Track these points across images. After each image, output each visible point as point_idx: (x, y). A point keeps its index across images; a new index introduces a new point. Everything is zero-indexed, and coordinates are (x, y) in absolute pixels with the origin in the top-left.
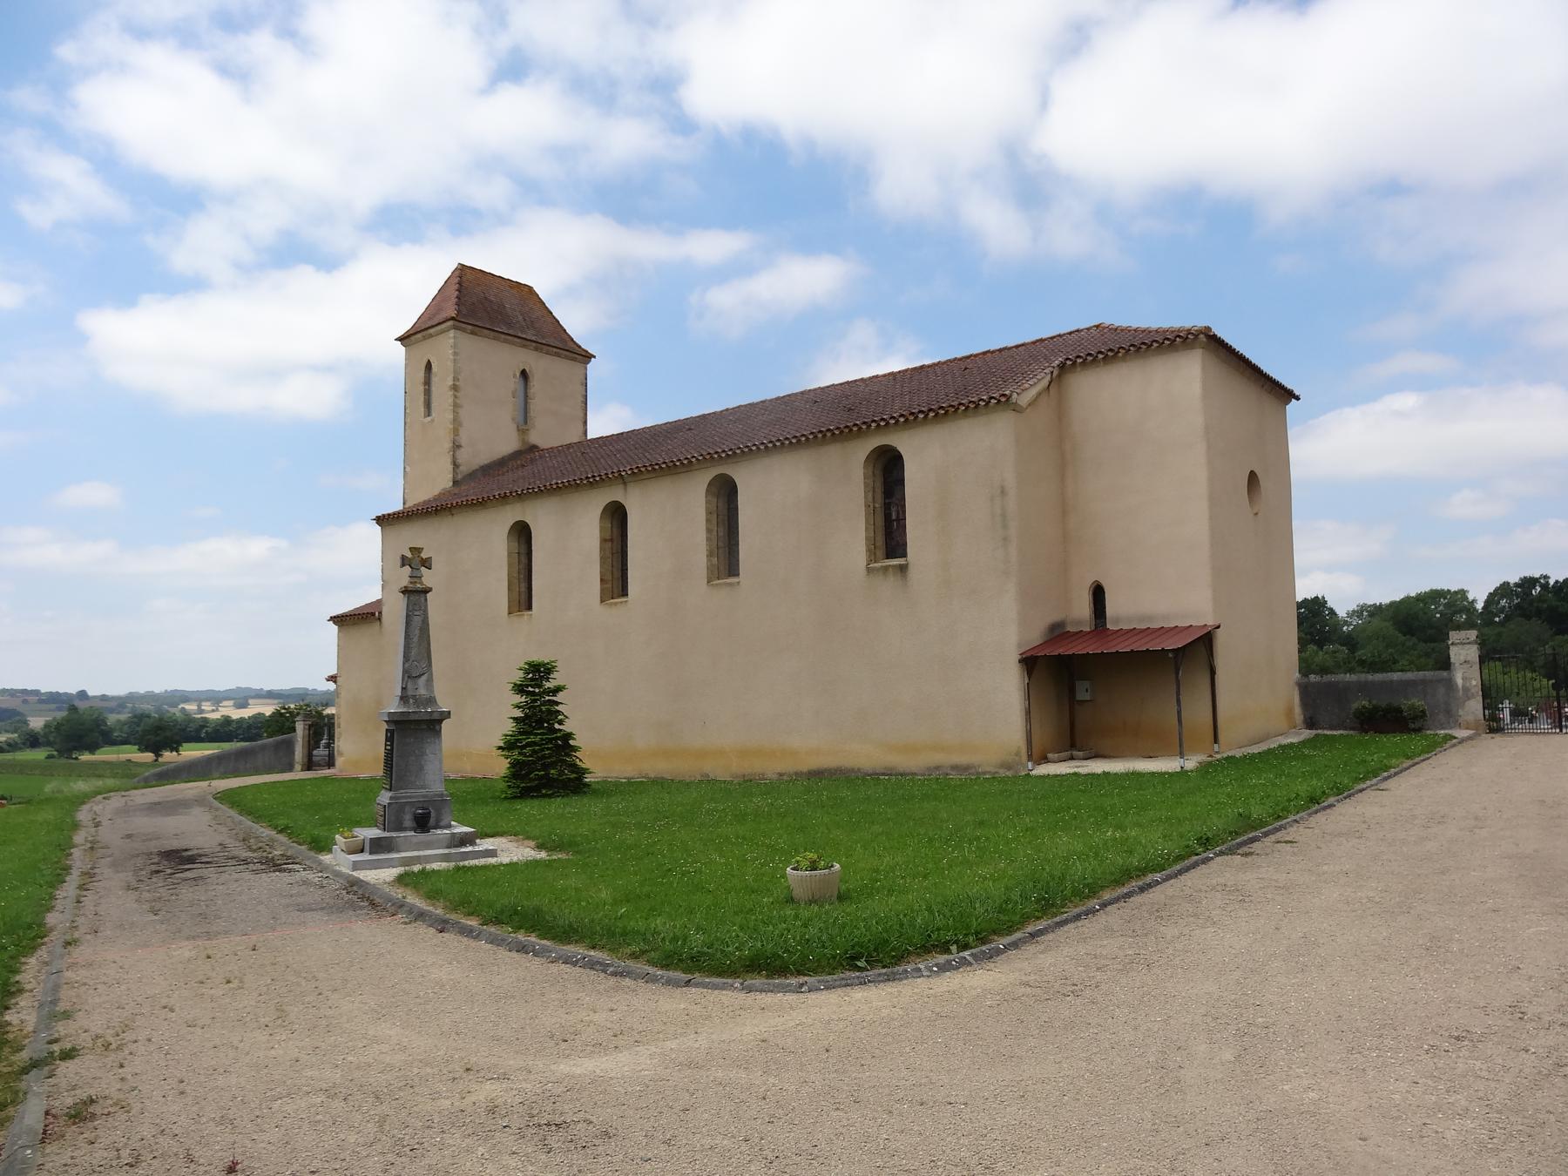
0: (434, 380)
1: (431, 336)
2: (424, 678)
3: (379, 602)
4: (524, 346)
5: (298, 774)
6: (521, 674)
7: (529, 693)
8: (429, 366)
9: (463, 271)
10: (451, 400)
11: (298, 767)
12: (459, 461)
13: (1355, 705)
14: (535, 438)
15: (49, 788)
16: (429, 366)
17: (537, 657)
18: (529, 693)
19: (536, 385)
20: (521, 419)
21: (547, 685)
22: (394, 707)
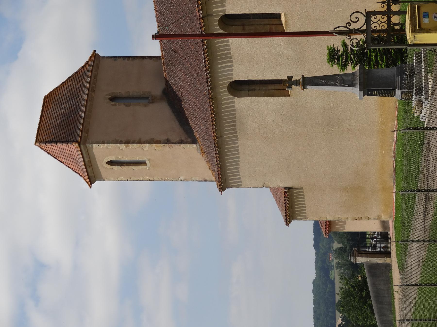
0: (121, 158)
1: (90, 161)
2: (344, 77)
3: (274, 191)
4: (92, 99)
5: (394, 261)
6: (336, 65)
7: (346, 60)
8: (110, 163)
9: (39, 140)
10: (136, 146)
11: (388, 260)
12: (178, 140)
13: (382, 215)
14: (158, 91)
15: (384, 64)
16: (110, 163)
17: (325, 57)
18: (346, 60)
19: (120, 91)
20: (146, 101)
21: (341, 50)
22: (357, 90)
